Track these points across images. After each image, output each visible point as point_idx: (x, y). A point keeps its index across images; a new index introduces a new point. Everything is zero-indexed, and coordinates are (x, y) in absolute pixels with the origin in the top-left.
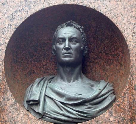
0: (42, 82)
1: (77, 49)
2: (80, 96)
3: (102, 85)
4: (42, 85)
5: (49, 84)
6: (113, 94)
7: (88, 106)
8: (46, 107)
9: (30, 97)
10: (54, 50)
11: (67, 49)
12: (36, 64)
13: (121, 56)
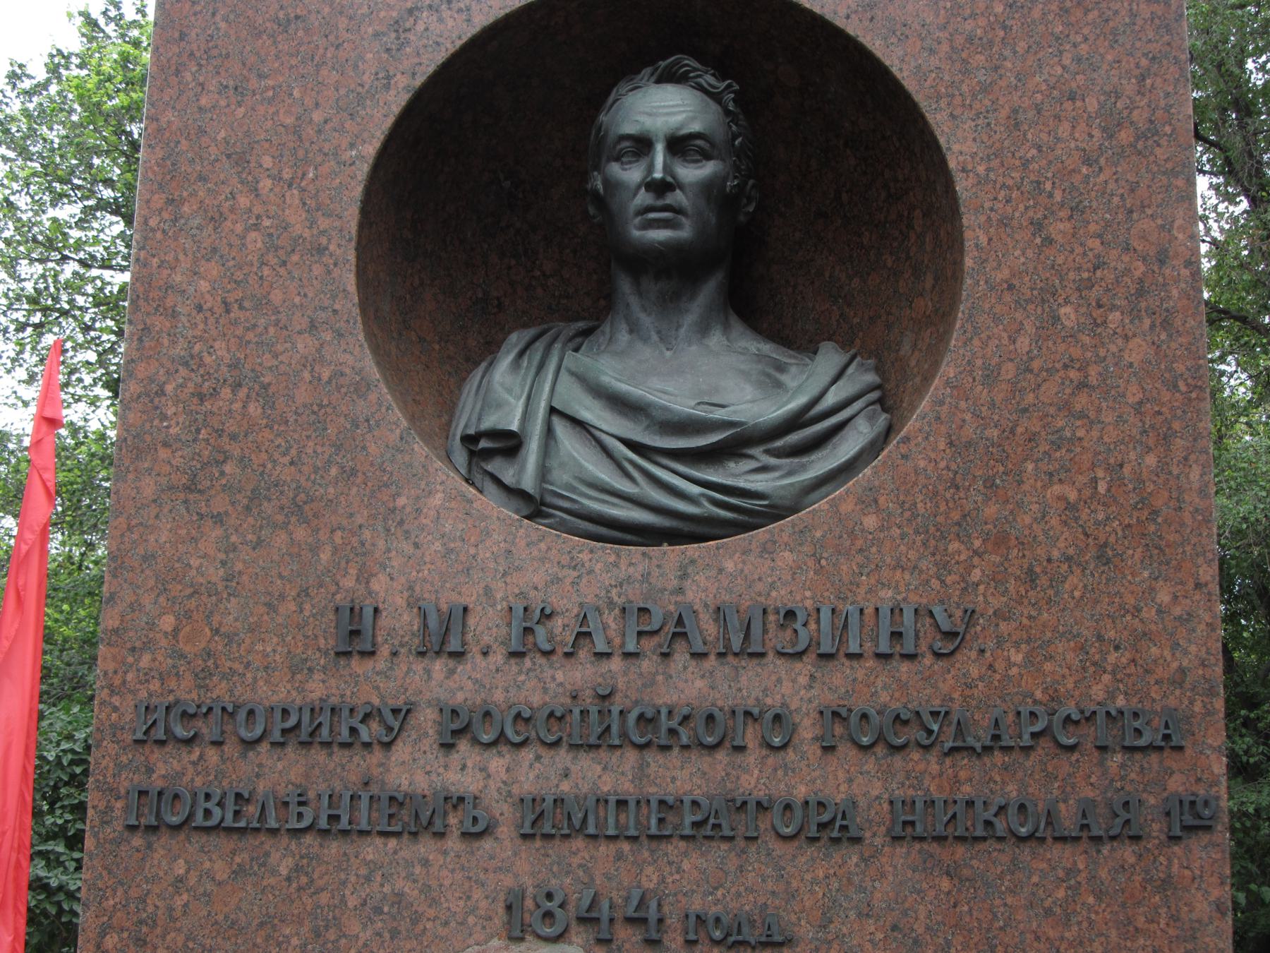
0: (540, 346)
1: (708, 188)
2: (719, 414)
3: (829, 359)
4: (535, 363)
5: (571, 359)
6: (878, 407)
7: (757, 459)
8: (553, 463)
9: (479, 419)
10: (595, 194)
11: (661, 188)
12: (509, 268)
13: (919, 230)
